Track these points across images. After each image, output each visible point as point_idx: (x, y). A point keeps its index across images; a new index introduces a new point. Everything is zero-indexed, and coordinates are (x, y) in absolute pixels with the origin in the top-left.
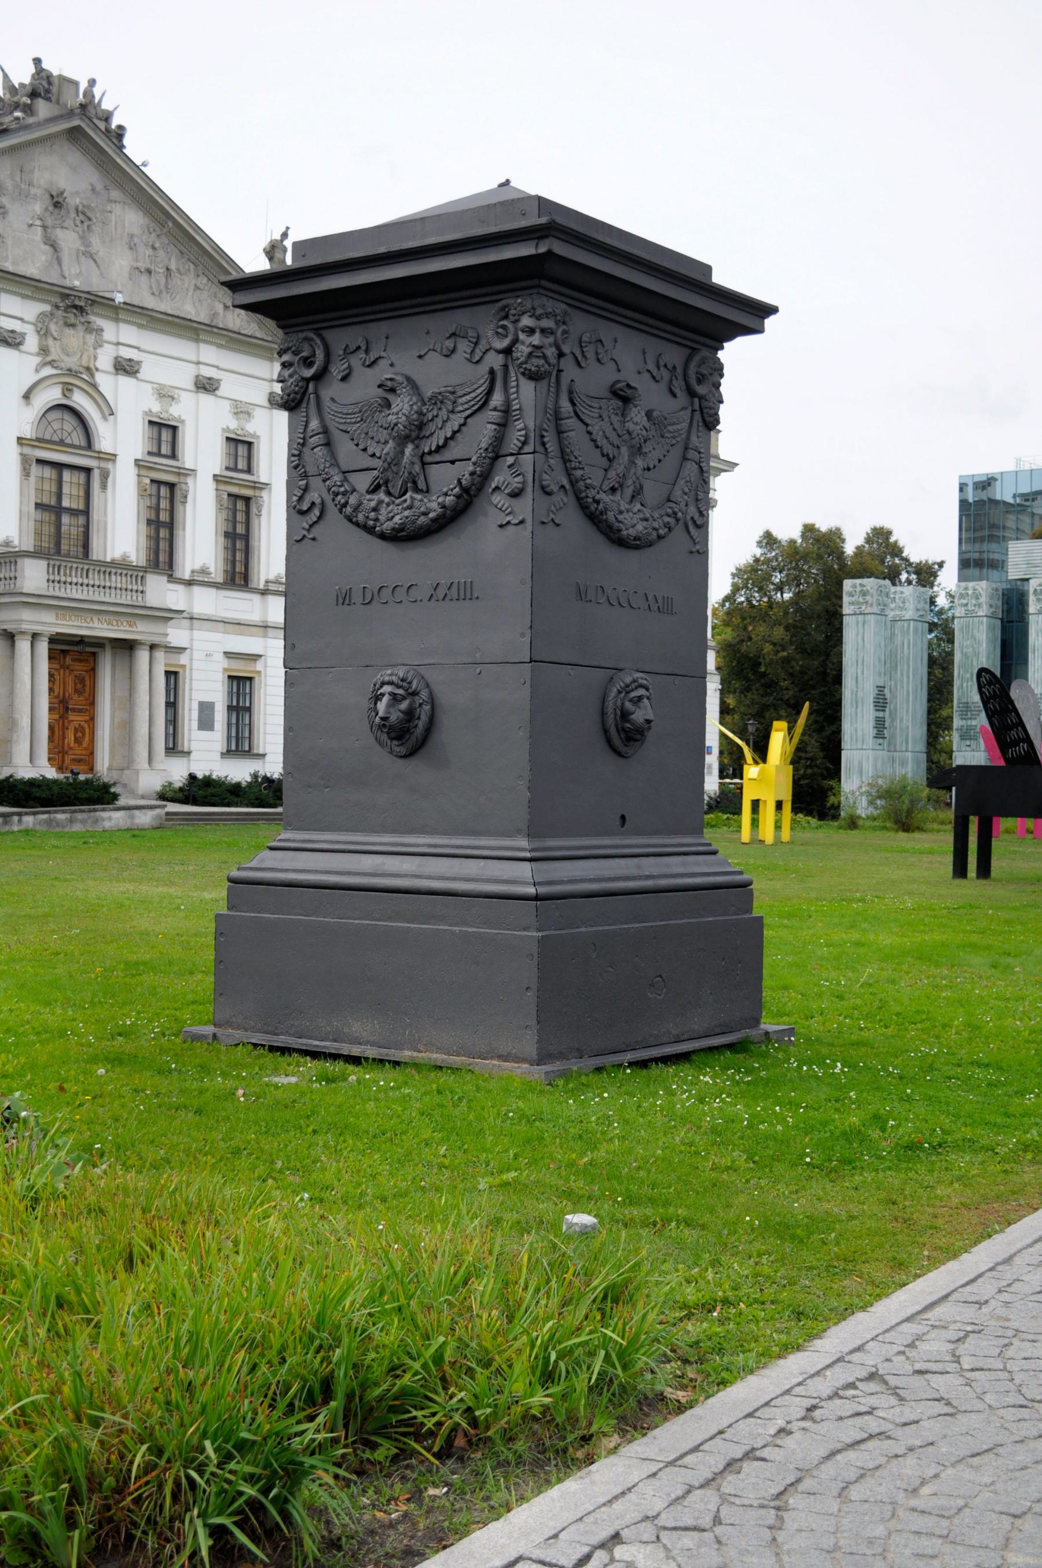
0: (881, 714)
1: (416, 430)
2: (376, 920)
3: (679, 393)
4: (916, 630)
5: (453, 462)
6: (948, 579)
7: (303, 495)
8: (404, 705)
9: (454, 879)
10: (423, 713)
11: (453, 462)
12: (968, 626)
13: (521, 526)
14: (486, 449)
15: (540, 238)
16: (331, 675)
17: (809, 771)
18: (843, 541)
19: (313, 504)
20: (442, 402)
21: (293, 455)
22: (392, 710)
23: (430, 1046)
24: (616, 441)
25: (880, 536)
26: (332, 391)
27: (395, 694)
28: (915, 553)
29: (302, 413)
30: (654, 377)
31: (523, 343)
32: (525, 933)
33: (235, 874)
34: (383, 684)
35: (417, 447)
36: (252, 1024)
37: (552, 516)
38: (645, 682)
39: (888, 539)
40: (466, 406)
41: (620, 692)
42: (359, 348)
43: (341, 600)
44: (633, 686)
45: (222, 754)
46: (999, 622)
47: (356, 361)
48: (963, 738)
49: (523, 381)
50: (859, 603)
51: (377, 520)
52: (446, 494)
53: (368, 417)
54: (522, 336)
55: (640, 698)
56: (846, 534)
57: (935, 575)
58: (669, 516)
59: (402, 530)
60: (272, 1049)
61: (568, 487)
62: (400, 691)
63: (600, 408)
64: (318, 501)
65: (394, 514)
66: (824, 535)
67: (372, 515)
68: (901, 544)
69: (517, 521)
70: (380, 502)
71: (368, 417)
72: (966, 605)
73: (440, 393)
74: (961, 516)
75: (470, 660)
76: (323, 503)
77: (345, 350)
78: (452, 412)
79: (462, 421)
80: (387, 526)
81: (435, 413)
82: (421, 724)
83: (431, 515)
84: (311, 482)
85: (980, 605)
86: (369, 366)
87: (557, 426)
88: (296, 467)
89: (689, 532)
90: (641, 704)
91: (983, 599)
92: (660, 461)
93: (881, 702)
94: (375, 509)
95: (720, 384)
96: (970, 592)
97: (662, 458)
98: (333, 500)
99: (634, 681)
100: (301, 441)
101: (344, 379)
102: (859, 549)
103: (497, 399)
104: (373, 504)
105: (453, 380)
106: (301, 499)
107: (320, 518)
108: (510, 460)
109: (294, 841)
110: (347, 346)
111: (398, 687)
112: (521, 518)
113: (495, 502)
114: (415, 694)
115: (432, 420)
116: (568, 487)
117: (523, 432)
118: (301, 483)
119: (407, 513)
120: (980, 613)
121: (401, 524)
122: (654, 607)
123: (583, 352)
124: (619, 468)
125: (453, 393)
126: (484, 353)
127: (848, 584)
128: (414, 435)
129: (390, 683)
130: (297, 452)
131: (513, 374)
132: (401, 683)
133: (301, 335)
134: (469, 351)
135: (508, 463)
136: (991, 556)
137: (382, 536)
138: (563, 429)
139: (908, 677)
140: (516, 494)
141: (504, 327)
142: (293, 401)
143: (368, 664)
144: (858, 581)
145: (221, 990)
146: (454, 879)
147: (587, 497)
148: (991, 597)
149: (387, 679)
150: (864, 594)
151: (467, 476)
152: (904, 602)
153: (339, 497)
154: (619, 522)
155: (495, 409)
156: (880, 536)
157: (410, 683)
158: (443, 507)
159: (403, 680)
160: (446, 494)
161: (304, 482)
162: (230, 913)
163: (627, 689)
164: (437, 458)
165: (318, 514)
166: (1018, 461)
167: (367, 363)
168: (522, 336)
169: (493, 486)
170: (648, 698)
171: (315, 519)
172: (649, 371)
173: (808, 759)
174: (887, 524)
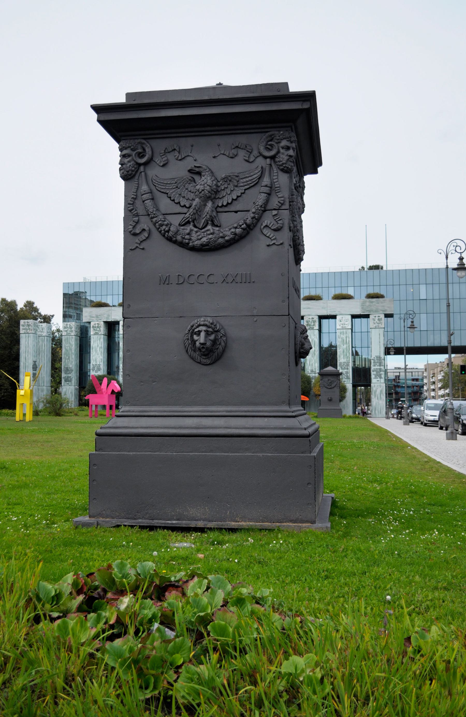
0: (35, 372)
1: (213, 194)
2: (203, 452)
4: (47, 340)
5: (236, 212)
6: (58, 322)
7: (136, 225)
8: (212, 337)
9: (253, 428)
11: (236, 212)
12: (67, 339)
13: (281, 246)
14: (261, 206)
15: (304, 101)
16: (156, 322)
17: (6, 394)
18: (17, 305)
20: (230, 181)
21: (129, 204)
23: (244, 519)
25: (30, 304)
26: (154, 172)
27: (208, 331)
28: (43, 311)
29: (134, 183)
31: (283, 154)
32: (303, 455)
33: (99, 431)
34: (200, 325)
36: (117, 514)
39: (33, 305)
40: (246, 184)
46: (78, 338)
47: (171, 157)
48: (66, 381)
49: (280, 173)
50: (26, 329)
51: (190, 239)
52: (236, 228)
53: (181, 186)
54: (282, 151)
56: (18, 303)
57: (50, 320)
59: (208, 245)
60: (142, 527)
62: (210, 330)
64: (147, 229)
65: (200, 238)
66: (10, 303)
67: (187, 237)
68: (38, 307)
70: (191, 230)
71: (181, 186)
72: (67, 331)
73: (230, 176)
74: (64, 298)
75: (249, 314)
77: (165, 151)
78: (237, 186)
80: (197, 243)
84: (140, 219)
85: (72, 331)
86: (180, 160)
88: (130, 211)
91: (73, 329)
93: (35, 367)
96: (68, 326)
100: (135, 197)
102: (21, 309)
103: (266, 180)
104: (188, 231)
105: (237, 170)
106: (134, 227)
108: (275, 212)
109: (133, 411)
110: (166, 149)
111: (209, 327)
112: (281, 242)
113: (265, 233)
115: (224, 190)
117: (282, 199)
118: (134, 219)
119: (210, 236)
120: (72, 334)
121: (208, 242)
125: (237, 176)
126: (256, 158)
127: (22, 322)
128: (213, 196)
129: (203, 325)
130: (132, 203)
131: (275, 169)
132: (211, 325)
133: (137, 141)
134: (248, 156)
135: (273, 214)
136: (70, 313)
139: (44, 358)
141: (271, 145)
142: (130, 175)
143: (181, 316)
144: (26, 321)
145: (93, 496)
146: (253, 428)
148: (76, 328)
149: (202, 323)
150: (29, 325)
151: (250, 218)
152: (42, 329)
153: (164, 227)
155: (266, 186)
156: (30, 304)
158: (235, 234)
159: (212, 324)
160: (236, 228)
161: (137, 218)
162: (97, 453)
164: (226, 209)
165: (147, 235)
166: (85, 278)
167: (180, 158)
168: (282, 151)
169: (264, 225)
171: (144, 238)
173: (5, 389)
174: (32, 300)
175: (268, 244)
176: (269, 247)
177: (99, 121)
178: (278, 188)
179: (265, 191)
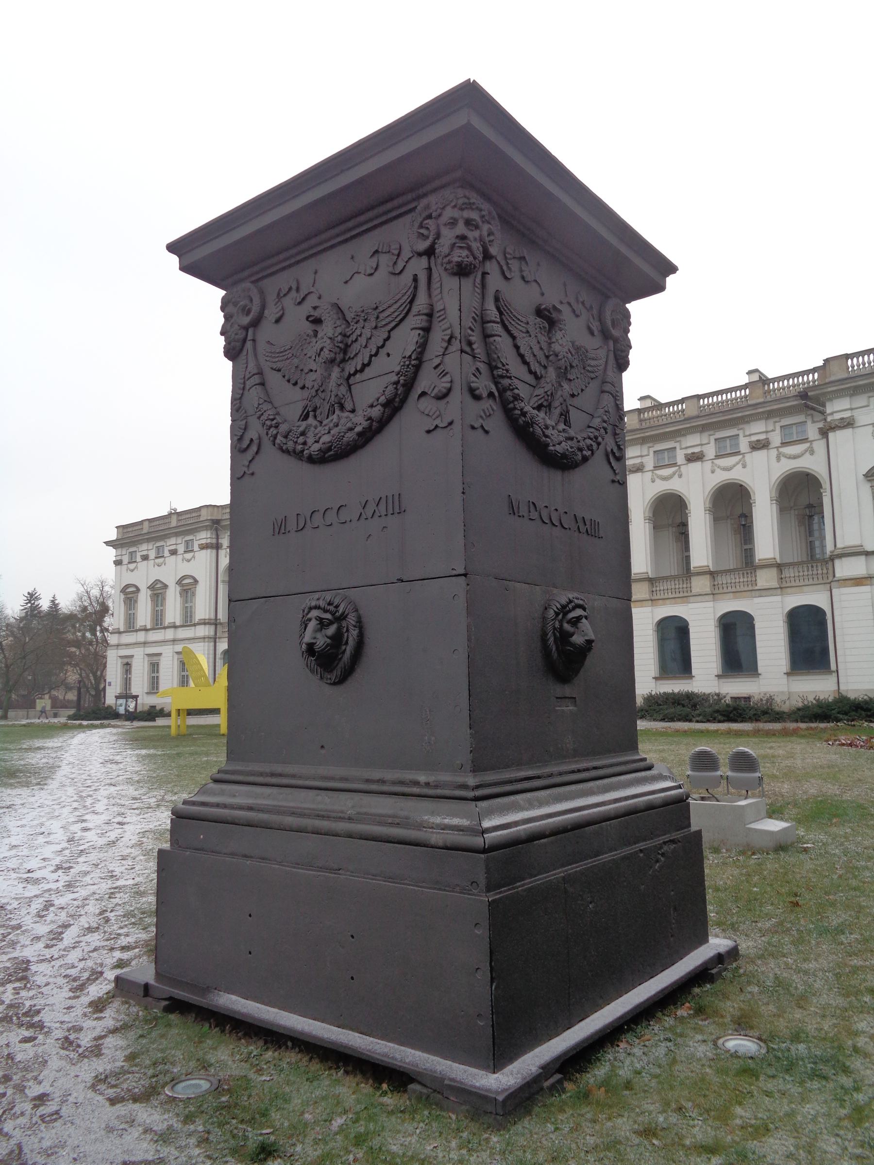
3: (596, 333)
8: (331, 630)
10: (351, 639)
14: (410, 357)
19: (252, 440)
22: (319, 635)
24: (544, 361)
30: (574, 311)
34: (311, 609)
35: (343, 370)
37: (481, 421)
38: (581, 602)
41: (557, 614)
42: (290, 289)
43: (277, 530)
44: (570, 606)
45: (656, 678)
47: (288, 302)
52: (372, 406)
55: (579, 619)
58: (591, 439)
59: (329, 449)
61: (496, 394)
62: (328, 616)
63: (528, 323)
65: (321, 436)
67: (301, 439)
69: (446, 425)
76: (260, 438)
79: (385, 336)
81: (358, 332)
82: (349, 649)
83: (359, 429)
87: (483, 329)
89: (610, 463)
90: (580, 625)
92: (582, 390)
94: (303, 434)
95: (629, 331)
97: (584, 388)
98: (267, 434)
99: (571, 601)
101: (278, 321)
107: (257, 453)
111: (326, 611)
112: (449, 420)
114: (343, 617)
115: (356, 340)
116: (496, 394)
122: (583, 529)
123: (507, 264)
124: (547, 386)
126: (407, 262)
129: (317, 607)
137: (311, 460)
138: (489, 332)
140: (443, 396)
147: (515, 408)
149: (313, 604)
154: (547, 436)
157: (337, 607)
159: (330, 604)
160: (372, 406)
163: (564, 610)
170: (586, 618)
172: (569, 304)
175: (427, 429)
176: (430, 435)
177: (184, 268)
178: (442, 312)
179: (417, 326)
